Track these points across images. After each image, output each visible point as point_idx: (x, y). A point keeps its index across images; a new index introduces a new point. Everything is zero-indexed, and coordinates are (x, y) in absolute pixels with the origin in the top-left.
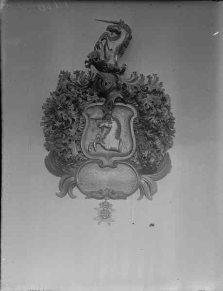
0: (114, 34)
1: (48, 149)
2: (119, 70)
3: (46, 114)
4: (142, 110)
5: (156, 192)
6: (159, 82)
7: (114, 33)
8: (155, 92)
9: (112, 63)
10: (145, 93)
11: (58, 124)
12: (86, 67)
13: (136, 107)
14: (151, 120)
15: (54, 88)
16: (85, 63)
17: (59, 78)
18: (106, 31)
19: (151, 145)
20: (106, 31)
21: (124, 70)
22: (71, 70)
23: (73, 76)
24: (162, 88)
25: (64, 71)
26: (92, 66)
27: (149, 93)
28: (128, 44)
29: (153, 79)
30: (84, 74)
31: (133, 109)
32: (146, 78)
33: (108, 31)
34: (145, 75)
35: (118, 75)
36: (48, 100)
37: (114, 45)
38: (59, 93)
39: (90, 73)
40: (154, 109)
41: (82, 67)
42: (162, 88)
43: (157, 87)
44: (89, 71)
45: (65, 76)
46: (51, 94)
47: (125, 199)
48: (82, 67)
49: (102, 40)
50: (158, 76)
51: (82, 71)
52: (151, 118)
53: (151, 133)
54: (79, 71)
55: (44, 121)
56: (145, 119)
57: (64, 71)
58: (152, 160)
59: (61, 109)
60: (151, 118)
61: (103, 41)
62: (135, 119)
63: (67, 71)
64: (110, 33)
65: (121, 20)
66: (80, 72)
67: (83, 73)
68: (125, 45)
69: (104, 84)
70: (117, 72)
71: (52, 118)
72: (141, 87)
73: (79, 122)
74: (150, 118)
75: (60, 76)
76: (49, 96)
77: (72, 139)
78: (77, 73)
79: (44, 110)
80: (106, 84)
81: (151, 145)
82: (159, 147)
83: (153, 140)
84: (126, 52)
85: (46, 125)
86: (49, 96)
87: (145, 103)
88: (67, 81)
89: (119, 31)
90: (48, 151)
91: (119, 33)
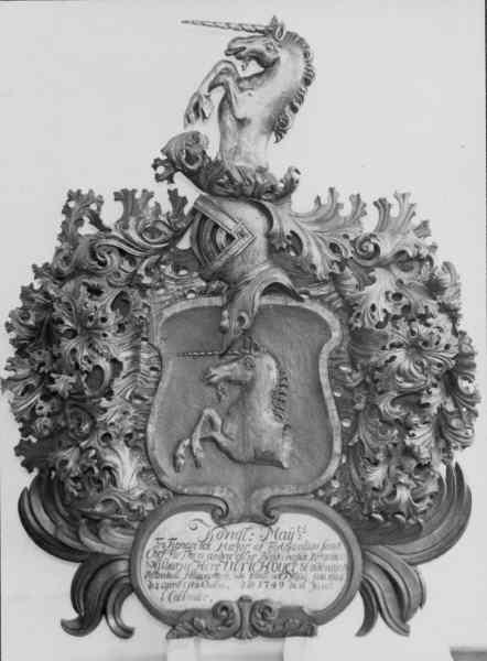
0: (254, 68)
1: (28, 465)
2: (273, 189)
3: (22, 349)
4: (359, 325)
5: (421, 604)
6: (416, 221)
7: (254, 62)
8: (402, 260)
9: (83, 228)
10: (369, 263)
11: (62, 384)
12: (158, 178)
13: (336, 311)
14: (394, 365)
15: (45, 250)
16: (155, 167)
17: (64, 218)
18: (225, 58)
19: (395, 445)
20: (225, 58)
21: (291, 186)
22: (104, 186)
23: (111, 213)
24: (428, 241)
25: (79, 191)
26: (179, 178)
27: (385, 265)
28: (301, 100)
29: (394, 212)
30: (151, 204)
31: (327, 315)
32: (229, 59)
33: (232, 59)
34: (369, 199)
35: (267, 204)
36: (26, 294)
37: (254, 104)
38: (66, 269)
39: (173, 195)
40: (402, 323)
41: (142, 179)
42: (428, 241)
43: (409, 242)
44: (169, 192)
45: (80, 207)
46: (38, 272)
47: (311, 633)
48: (142, 179)
49: (211, 88)
50: (410, 200)
51: (144, 191)
52: (393, 358)
53: (393, 403)
54: (134, 191)
55: (12, 374)
56: (373, 359)
57: (79, 191)
58: (403, 495)
59: (73, 334)
60: (393, 358)
61: (215, 90)
62: (338, 351)
63: (91, 191)
64: (239, 64)
65: (274, 19)
66: (138, 196)
67: (148, 195)
68: (293, 102)
69: (221, 238)
70: (267, 195)
71: (42, 364)
72: (353, 243)
73: (137, 371)
74: (388, 354)
75: (67, 210)
76: (29, 279)
77: (111, 430)
78: (124, 196)
79: (13, 335)
80: (230, 238)
81: (395, 445)
82: (425, 454)
83: (406, 427)
84: (297, 123)
85: (20, 387)
86: (29, 279)
87: (369, 305)
88: (87, 229)
89: (270, 56)
90: (30, 471)
91: (268, 66)
